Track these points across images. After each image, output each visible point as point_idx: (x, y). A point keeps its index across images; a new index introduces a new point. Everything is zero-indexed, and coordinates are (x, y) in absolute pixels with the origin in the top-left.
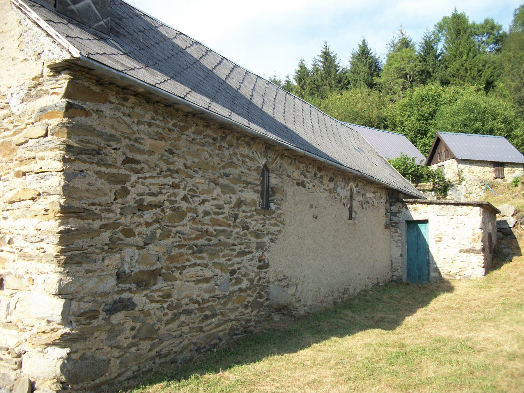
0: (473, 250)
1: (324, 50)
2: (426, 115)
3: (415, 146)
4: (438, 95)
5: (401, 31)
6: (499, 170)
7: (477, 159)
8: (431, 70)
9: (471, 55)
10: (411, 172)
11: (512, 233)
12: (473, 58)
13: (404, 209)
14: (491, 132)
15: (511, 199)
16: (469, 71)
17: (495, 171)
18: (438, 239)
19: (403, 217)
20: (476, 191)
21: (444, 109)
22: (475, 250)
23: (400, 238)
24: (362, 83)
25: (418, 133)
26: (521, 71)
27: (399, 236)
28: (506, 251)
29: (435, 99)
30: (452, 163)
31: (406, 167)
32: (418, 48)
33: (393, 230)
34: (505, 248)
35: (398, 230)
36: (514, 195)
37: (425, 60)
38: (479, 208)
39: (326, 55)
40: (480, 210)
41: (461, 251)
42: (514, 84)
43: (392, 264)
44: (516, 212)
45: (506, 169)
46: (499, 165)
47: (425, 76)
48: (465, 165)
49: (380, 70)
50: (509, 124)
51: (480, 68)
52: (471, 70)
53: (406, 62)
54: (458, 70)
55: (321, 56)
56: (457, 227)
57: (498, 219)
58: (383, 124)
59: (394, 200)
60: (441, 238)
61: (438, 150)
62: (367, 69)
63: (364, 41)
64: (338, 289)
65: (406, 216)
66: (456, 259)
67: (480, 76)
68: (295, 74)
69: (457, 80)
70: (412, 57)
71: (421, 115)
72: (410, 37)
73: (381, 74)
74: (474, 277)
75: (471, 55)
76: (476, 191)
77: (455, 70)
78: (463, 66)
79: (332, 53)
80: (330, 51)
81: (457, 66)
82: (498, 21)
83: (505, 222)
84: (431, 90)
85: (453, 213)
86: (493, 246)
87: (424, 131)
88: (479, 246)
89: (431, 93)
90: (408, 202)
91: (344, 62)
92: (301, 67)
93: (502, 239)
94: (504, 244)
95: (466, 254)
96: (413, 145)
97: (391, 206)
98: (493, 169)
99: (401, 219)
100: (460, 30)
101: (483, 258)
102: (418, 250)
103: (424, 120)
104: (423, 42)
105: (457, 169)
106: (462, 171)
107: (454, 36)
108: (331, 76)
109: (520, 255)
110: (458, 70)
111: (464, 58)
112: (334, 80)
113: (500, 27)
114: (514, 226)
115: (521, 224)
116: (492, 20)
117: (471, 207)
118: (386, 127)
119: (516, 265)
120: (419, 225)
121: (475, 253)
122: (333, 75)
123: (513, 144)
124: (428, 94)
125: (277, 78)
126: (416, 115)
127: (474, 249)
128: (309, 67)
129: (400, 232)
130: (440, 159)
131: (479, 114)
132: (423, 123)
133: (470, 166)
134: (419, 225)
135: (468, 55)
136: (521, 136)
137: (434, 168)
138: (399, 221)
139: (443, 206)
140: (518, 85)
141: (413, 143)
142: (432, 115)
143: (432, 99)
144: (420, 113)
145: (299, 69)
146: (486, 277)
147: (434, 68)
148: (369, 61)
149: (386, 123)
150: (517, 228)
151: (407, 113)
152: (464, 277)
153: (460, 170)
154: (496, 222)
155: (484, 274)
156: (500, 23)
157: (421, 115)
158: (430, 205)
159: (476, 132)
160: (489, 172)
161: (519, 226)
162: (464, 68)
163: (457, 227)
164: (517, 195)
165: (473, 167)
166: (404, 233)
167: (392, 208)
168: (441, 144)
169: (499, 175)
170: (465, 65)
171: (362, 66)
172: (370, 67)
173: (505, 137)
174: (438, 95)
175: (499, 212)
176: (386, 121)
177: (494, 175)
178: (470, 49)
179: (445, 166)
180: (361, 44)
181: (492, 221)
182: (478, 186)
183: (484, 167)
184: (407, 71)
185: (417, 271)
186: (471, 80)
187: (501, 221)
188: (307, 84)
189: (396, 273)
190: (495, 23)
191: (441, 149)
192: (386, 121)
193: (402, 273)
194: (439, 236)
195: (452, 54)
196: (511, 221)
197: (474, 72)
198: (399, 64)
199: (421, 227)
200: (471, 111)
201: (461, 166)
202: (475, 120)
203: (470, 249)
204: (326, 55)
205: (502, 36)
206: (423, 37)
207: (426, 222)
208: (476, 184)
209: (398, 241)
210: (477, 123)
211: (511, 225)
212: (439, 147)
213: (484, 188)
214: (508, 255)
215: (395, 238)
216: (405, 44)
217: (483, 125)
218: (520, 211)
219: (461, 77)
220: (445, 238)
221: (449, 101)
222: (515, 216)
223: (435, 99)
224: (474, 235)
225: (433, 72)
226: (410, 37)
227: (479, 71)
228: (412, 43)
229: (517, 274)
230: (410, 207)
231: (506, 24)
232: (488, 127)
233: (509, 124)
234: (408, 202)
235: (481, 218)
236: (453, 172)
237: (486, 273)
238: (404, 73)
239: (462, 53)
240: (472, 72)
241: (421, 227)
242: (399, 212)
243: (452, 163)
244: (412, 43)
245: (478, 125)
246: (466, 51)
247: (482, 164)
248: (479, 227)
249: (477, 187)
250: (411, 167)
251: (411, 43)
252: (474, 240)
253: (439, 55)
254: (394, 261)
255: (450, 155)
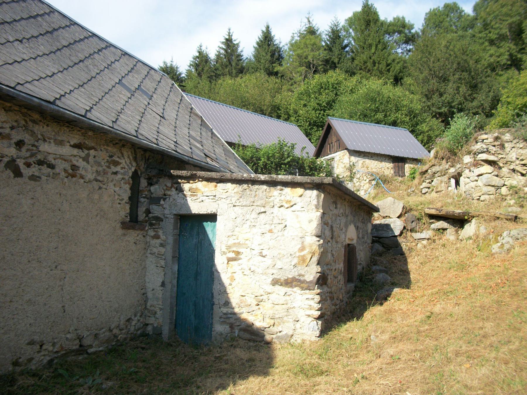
0: (299, 281)
1: (227, 37)
2: (324, 104)
3: (310, 140)
4: (339, 83)
5: (308, 19)
6: (398, 167)
7: (372, 151)
8: (336, 61)
9: (380, 47)
10: (289, 162)
11: (397, 246)
12: (382, 51)
13: (173, 192)
14: (394, 124)
15: (406, 197)
16: (377, 64)
17: (394, 168)
18: (232, 255)
19: (170, 206)
20: (365, 188)
21: (343, 98)
22: (304, 282)
23: (162, 250)
24: (262, 71)
25: (314, 125)
26: (430, 61)
27: (162, 245)
28: (380, 277)
29: (336, 87)
30: (343, 156)
31: (283, 155)
32: (324, 37)
33: (151, 233)
34: (381, 271)
35: (160, 233)
36: (409, 191)
37: (330, 50)
38: (315, 192)
39: (229, 42)
40: (318, 197)
41: (275, 282)
42: (421, 76)
43: (146, 301)
44: (406, 211)
45: (407, 166)
46: (399, 161)
47: (330, 65)
48: (357, 159)
49: (282, 58)
50: (414, 117)
51: (389, 62)
52: (379, 63)
53: (310, 49)
54: (365, 62)
55: (223, 43)
56: (270, 231)
57: (377, 222)
58: (276, 112)
59: (154, 172)
60: (238, 253)
61: (329, 140)
62: (268, 57)
63: (268, 27)
64: (147, 325)
65: (176, 205)
66: (265, 297)
67: (389, 70)
68: (192, 60)
69: (364, 73)
70: (316, 45)
71: (318, 104)
72: (317, 26)
73: (283, 63)
74: (297, 339)
75: (380, 47)
76: (365, 188)
77: (362, 62)
78: (370, 58)
79: (235, 40)
80: (234, 38)
81: (365, 58)
82: (409, 19)
83: (388, 226)
84: (332, 77)
85: (263, 202)
86: (359, 267)
87: (321, 122)
88: (312, 273)
89: (331, 80)
90: (181, 177)
91: (247, 49)
92: (199, 52)
93: (381, 255)
94: (382, 263)
95: (283, 290)
96: (307, 139)
97: (150, 184)
98: (391, 165)
99: (167, 212)
100: (370, 22)
101: (318, 298)
102: (197, 274)
103: (321, 110)
104: (330, 30)
105: (348, 162)
106: (354, 165)
107: (363, 27)
108: (232, 65)
109: (406, 284)
110: (365, 62)
111: (373, 50)
112: (235, 68)
113: (411, 27)
114: (401, 233)
115: (411, 231)
116: (403, 18)
117: (300, 191)
118: (279, 117)
119: (390, 312)
120: (205, 224)
121: (303, 289)
122: (234, 64)
123: (418, 140)
124: (328, 82)
125: (174, 64)
126: (313, 103)
127: (302, 278)
128: (212, 55)
129: (163, 237)
130: (330, 151)
131: (381, 103)
132: (320, 114)
133: (364, 160)
134: (205, 224)
135: (377, 46)
136: (427, 132)
137: (322, 160)
138: (164, 215)
139: (245, 186)
140: (426, 77)
141: (307, 136)
142: (330, 105)
143: (333, 87)
144: (317, 101)
145: (198, 54)
146: (323, 341)
147: (340, 59)
148: (271, 48)
149: (279, 112)
150: (405, 237)
151: (303, 102)
152: (278, 337)
153: (351, 163)
154: (370, 227)
155: (318, 333)
156: (412, 22)
157: (318, 104)
158: (220, 185)
159: (378, 122)
160: (386, 168)
161: (409, 233)
162: (372, 61)
163: (270, 231)
164: (413, 191)
165: (368, 161)
166: (171, 240)
167: (152, 188)
168: (332, 132)
169: (398, 173)
170: (373, 58)
171: (264, 54)
172: (272, 55)
173: (410, 132)
174: (339, 83)
175: (377, 210)
176: (280, 110)
177: (392, 172)
178: (379, 42)
179: (336, 159)
180: (264, 29)
181: (360, 225)
182: (368, 180)
183: (381, 161)
184: (310, 58)
185: (193, 317)
186: (379, 74)
187: (380, 225)
188: (205, 71)
189: (151, 320)
190: (407, 21)
191: (332, 138)
192: (280, 110)
193: (161, 319)
194: (235, 249)
195: (361, 46)
196: (397, 226)
197: (383, 66)
198: (302, 51)
199: (208, 226)
200: (373, 100)
201: (353, 159)
202: (377, 110)
203: (294, 279)
204: (229, 42)
205: (413, 36)
206: (330, 25)
207: (212, 217)
208: (365, 178)
209: (159, 256)
210: (377, 112)
211: (397, 233)
212: (329, 136)
213: (374, 183)
214: (382, 286)
215: (155, 250)
216: (312, 31)
217: (386, 116)
218: (411, 210)
219: (369, 69)
220: (245, 253)
221: (351, 90)
222: (403, 218)
223: (336, 88)
224: (302, 249)
225: (338, 63)
226: (317, 26)
227: (388, 65)
228: (319, 32)
229: (386, 337)
230: (186, 186)
231: (418, 23)
232: (392, 118)
233: (414, 117)
234: (181, 177)
235: (319, 214)
236: (343, 166)
237: (323, 332)
238: (307, 61)
239: (370, 46)
240: (380, 66)
241: (208, 226)
242: (165, 197)
243: (343, 156)
244: (319, 32)
245: (380, 116)
246: (374, 43)
247: (379, 157)
248: (314, 232)
249: (365, 182)
250: (288, 157)
251: (318, 33)
252: (303, 259)
253: (346, 46)
254: (150, 295)
255: (342, 146)
